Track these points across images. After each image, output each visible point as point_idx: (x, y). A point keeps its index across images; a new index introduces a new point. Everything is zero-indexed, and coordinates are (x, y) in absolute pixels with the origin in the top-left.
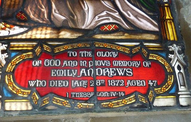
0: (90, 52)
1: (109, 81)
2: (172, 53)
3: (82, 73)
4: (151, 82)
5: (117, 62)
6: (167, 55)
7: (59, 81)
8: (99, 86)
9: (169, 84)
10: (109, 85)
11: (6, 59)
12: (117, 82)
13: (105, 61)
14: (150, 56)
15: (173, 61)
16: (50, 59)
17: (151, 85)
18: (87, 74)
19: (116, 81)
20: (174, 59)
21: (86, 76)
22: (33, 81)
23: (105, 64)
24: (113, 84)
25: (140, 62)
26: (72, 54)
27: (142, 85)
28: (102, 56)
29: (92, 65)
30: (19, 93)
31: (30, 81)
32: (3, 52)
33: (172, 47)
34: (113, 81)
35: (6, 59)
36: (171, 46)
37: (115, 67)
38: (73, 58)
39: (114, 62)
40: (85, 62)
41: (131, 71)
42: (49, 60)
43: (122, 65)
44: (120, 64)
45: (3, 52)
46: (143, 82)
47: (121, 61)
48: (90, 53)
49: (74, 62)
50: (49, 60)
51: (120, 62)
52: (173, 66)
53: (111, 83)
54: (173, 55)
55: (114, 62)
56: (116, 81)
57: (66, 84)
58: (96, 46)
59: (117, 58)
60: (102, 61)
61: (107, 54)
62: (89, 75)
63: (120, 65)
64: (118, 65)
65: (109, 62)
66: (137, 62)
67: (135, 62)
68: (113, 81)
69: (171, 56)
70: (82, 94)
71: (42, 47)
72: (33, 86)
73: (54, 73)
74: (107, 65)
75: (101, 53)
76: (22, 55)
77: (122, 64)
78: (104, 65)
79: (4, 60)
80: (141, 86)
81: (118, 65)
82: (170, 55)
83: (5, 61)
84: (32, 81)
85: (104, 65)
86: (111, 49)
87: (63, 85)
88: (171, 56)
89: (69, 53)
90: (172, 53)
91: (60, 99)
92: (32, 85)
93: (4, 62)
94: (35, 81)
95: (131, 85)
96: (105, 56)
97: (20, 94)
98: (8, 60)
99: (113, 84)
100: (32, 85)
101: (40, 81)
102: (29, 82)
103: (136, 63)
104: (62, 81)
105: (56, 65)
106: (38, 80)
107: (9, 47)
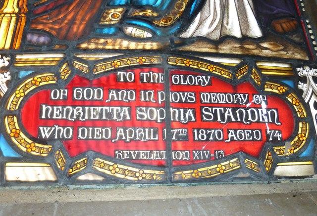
0: (160, 74)
1: (195, 131)
2: (304, 79)
3: (228, 116)
4: (278, 134)
5: (207, 96)
6: (296, 84)
7: (96, 129)
8: (220, 141)
9: (301, 139)
10: (196, 139)
11: (8, 83)
12: (210, 133)
13: (186, 93)
14: (266, 86)
15: (306, 94)
16: (83, 87)
17: (279, 139)
18: (236, 118)
19: (208, 132)
20: (308, 90)
21: (233, 122)
22: (49, 128)
23: (186, 99)
24: (203, 137)
25: (247, 95)
26: (125, 77)
27: (104, 137)
28: (182, 83)
29: (164, 100)
30: (32, 151)
31: (43, 126)
32: (4, 69)
33: (304, 69)
34: (202, 132)
35: (8, 83)
36: (302, 69)
37: (219, 105)
38: (126, 85)
39: (203, 95)
40: (150, 94)
41: (139, 115)
42: (81, 89)
43: (216, 102)
44: (214, 98)
45: (4, 69)
46: (107, 131)
47: (215, 94)
48: (162, 75)
49: (96, 90)
50: (81, 89)
51: (213, 95)
52: (306, 101)
53: (198, 134)
54: (305, 85)
55: (203, 95)
56: (208, 132)
57: (107, 135)
58: (87, 66)
59: (210, 89)
60: (181, 93)
61: (191, 79)
62: (239, 120)
63: (213, 102)
64: (210, 100)
65: (193, 94)
66: (242, 95)
67: (239, 96)
68: (202, 132)
69: (302, 86)
70: (126, 153)
71: (71, 65)
72: (48, 137)
73: (95, 113)
74: (189, 101)
75: (180, 77)
76: (35, 78)
77: (216, 98)
78: (184, 100)
79: (5, 84)
80: (102, 139)
81: (210, 100)
82: (300, 83)
83: (6, 86)
84: (47, 127)
85: (184, 100)
86: (199, 70)
87: (253, 137)
88: (302, 86)
89: (143, 75)
90: (304, 79)
91: (130, 168)
92: (46, 136)
93: (5, 89)
94: (53, 128)
95: (235, 139)
96: (186, 83)
97: (34, 151)
98: (13, 85)
99: (203, 137)
100: (46, 136)
101: (61, 128)
102: (41, 128)
103: (241, 97)
104: (100, 129)
105: (96, 97)
106: (57, 127)
107: (12, 62)
